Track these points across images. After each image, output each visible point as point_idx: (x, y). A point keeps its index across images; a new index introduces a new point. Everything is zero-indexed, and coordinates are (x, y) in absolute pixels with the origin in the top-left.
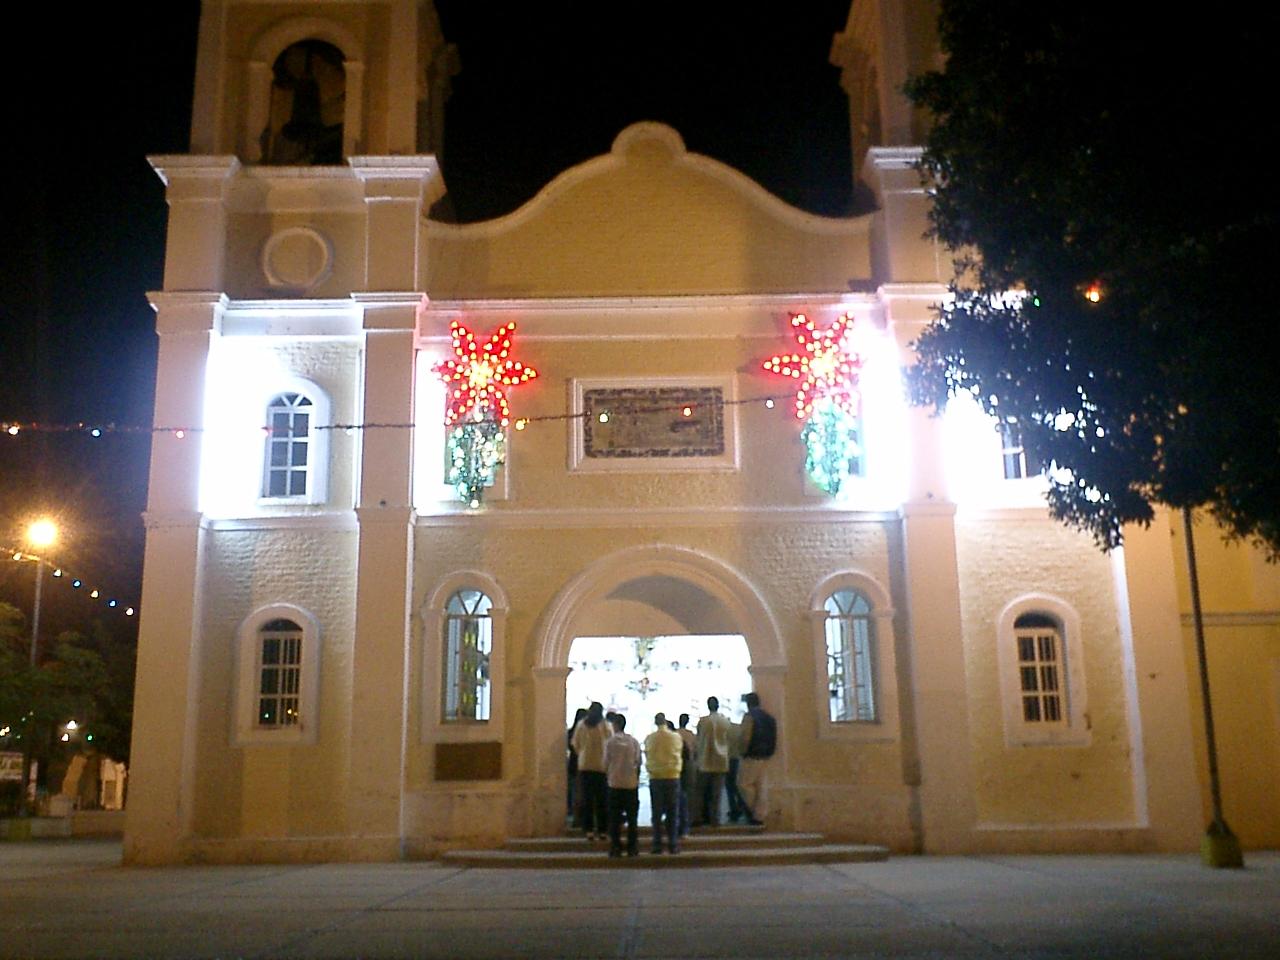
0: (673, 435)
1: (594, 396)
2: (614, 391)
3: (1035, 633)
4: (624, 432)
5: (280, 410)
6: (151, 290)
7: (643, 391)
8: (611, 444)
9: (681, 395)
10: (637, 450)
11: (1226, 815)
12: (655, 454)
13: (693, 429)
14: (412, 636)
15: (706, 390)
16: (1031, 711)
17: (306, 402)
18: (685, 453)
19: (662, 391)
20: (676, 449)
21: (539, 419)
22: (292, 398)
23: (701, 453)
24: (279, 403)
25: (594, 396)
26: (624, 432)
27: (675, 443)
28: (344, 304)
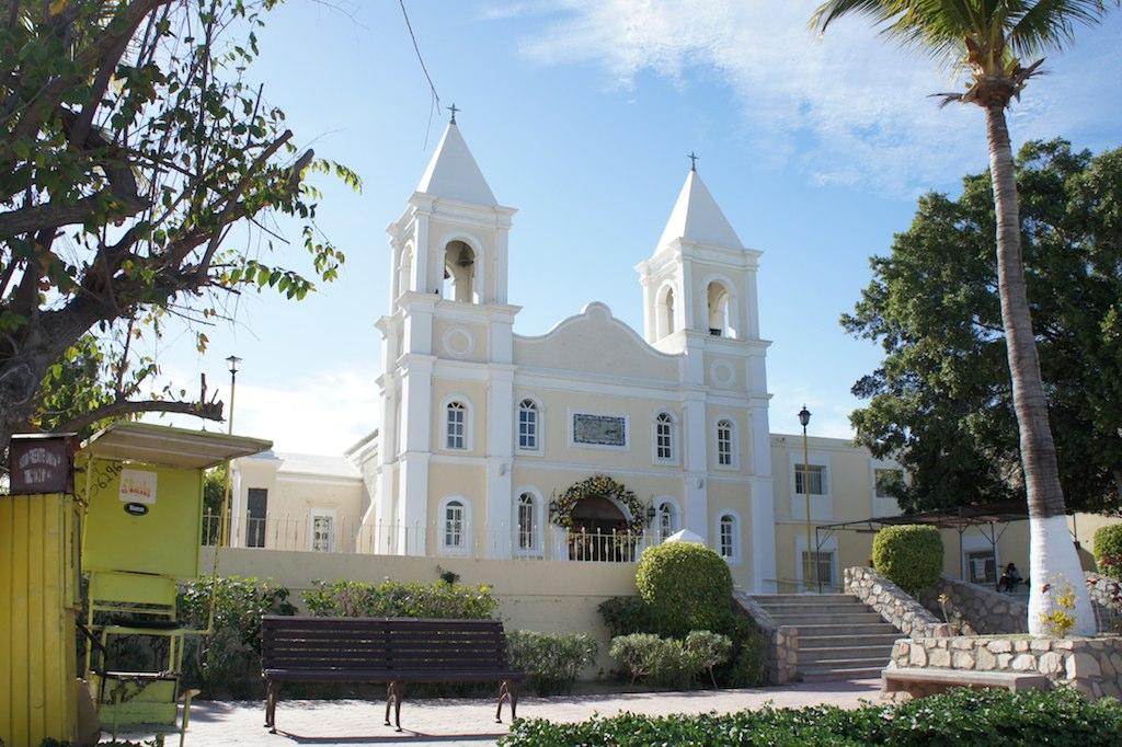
3: (454, 508)
22: (456, 405)
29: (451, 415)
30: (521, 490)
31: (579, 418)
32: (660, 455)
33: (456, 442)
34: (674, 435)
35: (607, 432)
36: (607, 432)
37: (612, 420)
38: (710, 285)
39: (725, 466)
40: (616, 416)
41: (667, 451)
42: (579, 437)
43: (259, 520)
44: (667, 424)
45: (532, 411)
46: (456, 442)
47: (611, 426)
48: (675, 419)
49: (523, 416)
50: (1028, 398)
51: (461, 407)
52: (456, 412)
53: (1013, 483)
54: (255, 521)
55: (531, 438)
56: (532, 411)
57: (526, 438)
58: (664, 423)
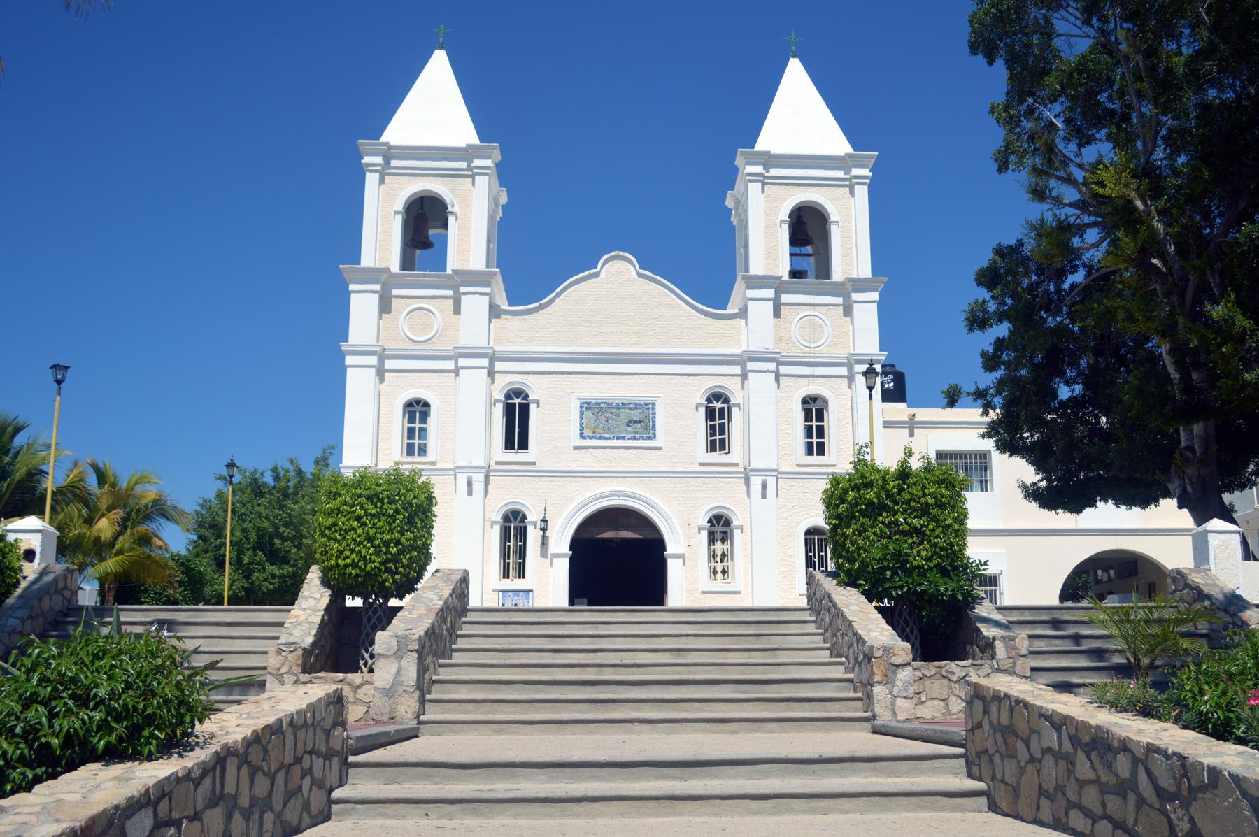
6: (1230, 489)
12: (618, 438)
17: (427, 405)
18: (635, 438)
36: (629, 423)
42: (587, 432)
47: (636, 415)
50: (1012, 710)
55: (722, 442)
56: (725, 529)
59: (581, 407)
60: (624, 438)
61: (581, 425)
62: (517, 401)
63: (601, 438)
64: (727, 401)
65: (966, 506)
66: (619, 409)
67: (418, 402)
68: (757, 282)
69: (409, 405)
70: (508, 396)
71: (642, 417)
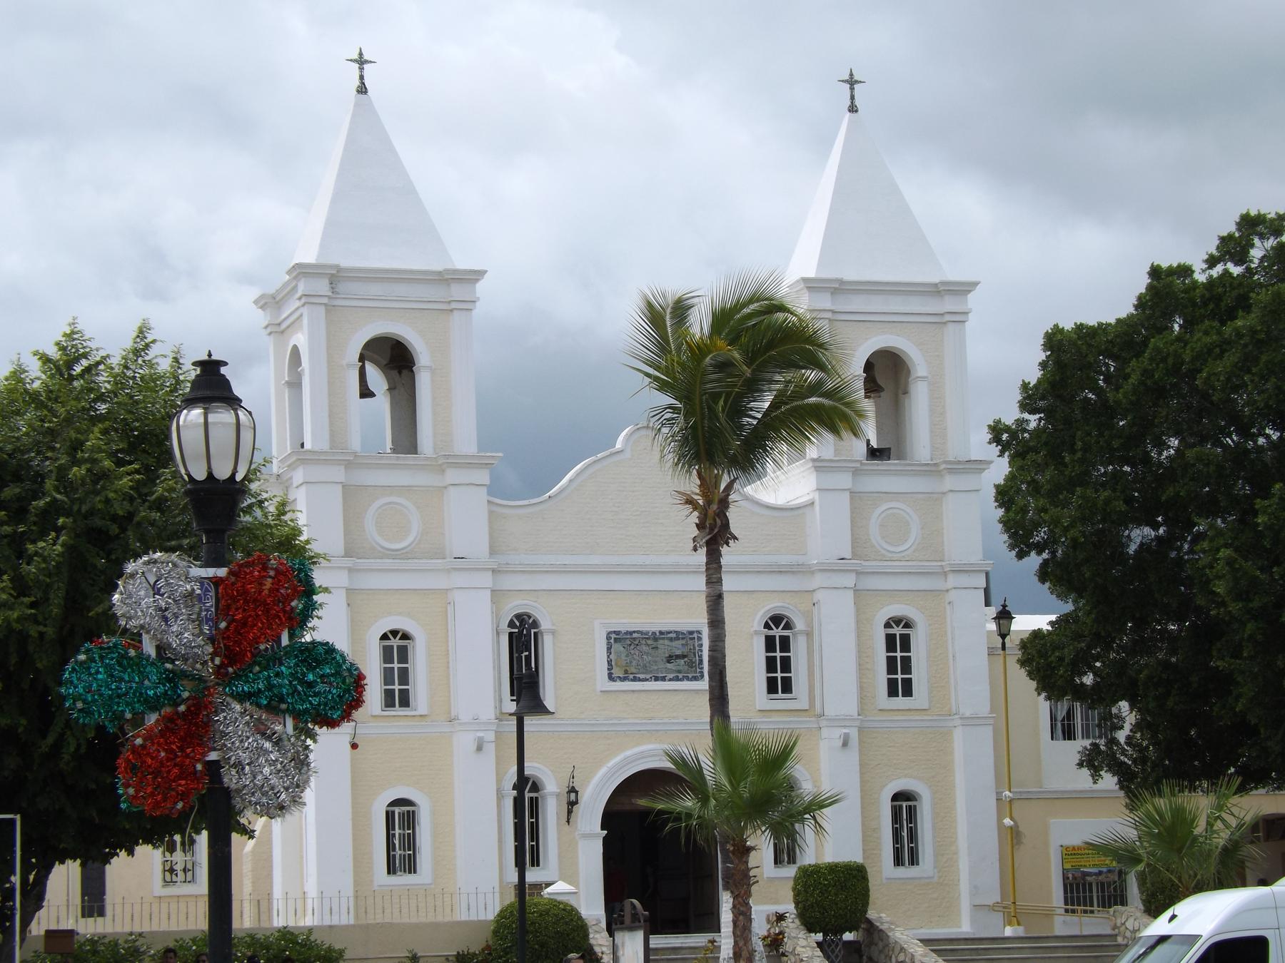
0: (669, 666)
1: (613, 636)
2: (627, 633)
4: (634, 663)
5: (387, 643)
7: (647, 633)
8: (626, 672)
9: (673, 635)
10: (642, 676)
11: (990, 903)
12: (657, 679)
13: (682, 662)
14: (571, 481)
15: (691, 633)
16: (772, 687)
17: (406, 636)
18: (677, 679)
19: (661, 633)
20: (671, 676)
21: (572, 804)
22: (394, 633)
23: (688, 679)
24: (384, 637)
25: (613, 636)
26: (634, 663)
27: (671, 671)
28: (119, 900)
29: (890, 642)
30: (513, 607)
31: (616, 638)
32: (892, 692)
33: (900, 687)
34: (798, 654)
35: (670, 659)
36: (670, 659)
37: (679, 635)
38: (869, 367)
39: (900, 702)
40: (685, 628)
41: (908, 685)
43: (904, 804)
44: (786, 633)
45: (786, 633)
46: (900, 687)
47: (677, 647)
48: (799, 625)
49: (770, 643)
51: (907, 626)
52: (898, 641)
53: (120, 792)
54: (901, 807)
56: (906, 631)
57: (526, 687)
58: (777, 632)
59: (608, 638)
60: (663, 679)
61: (609, 662)
62: (898, 631)
63: (635, 679)
64: (788, 626)
65: (1113, 321)
66: (656, 639)
67: (898, 621)
68: (971, 721)
69: (897, 797)
70: (887, 625)
71: (685, 650)
